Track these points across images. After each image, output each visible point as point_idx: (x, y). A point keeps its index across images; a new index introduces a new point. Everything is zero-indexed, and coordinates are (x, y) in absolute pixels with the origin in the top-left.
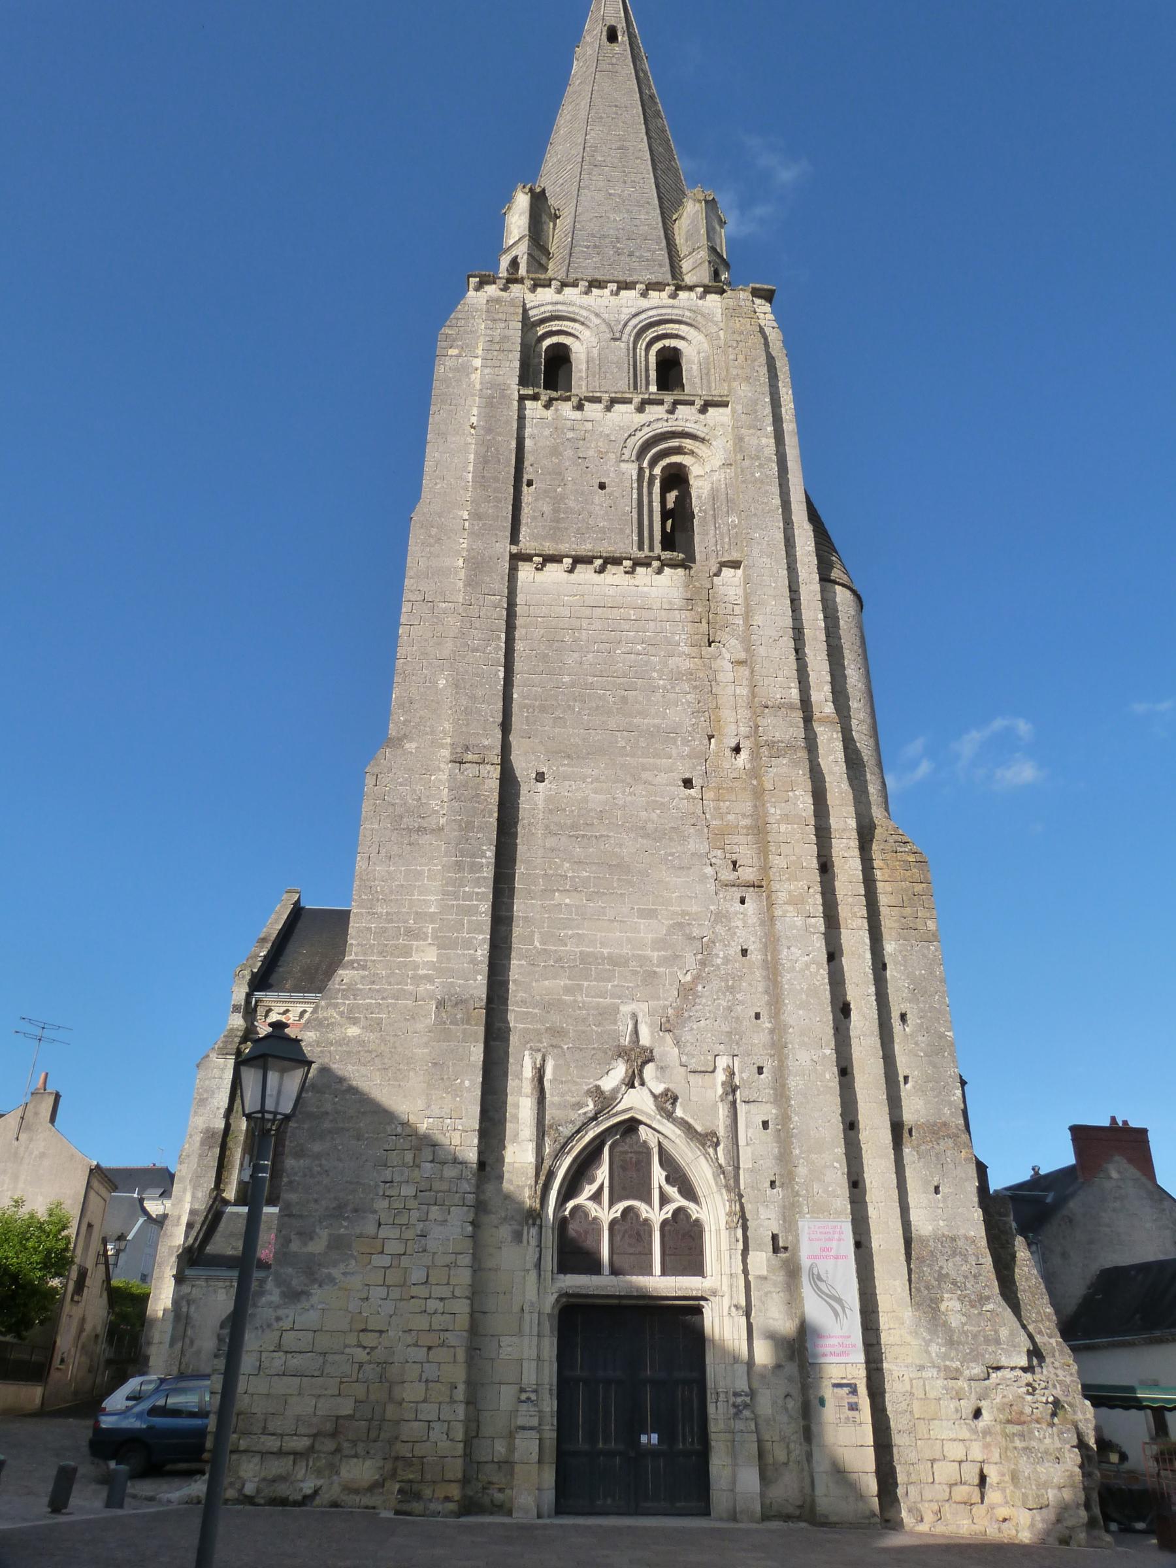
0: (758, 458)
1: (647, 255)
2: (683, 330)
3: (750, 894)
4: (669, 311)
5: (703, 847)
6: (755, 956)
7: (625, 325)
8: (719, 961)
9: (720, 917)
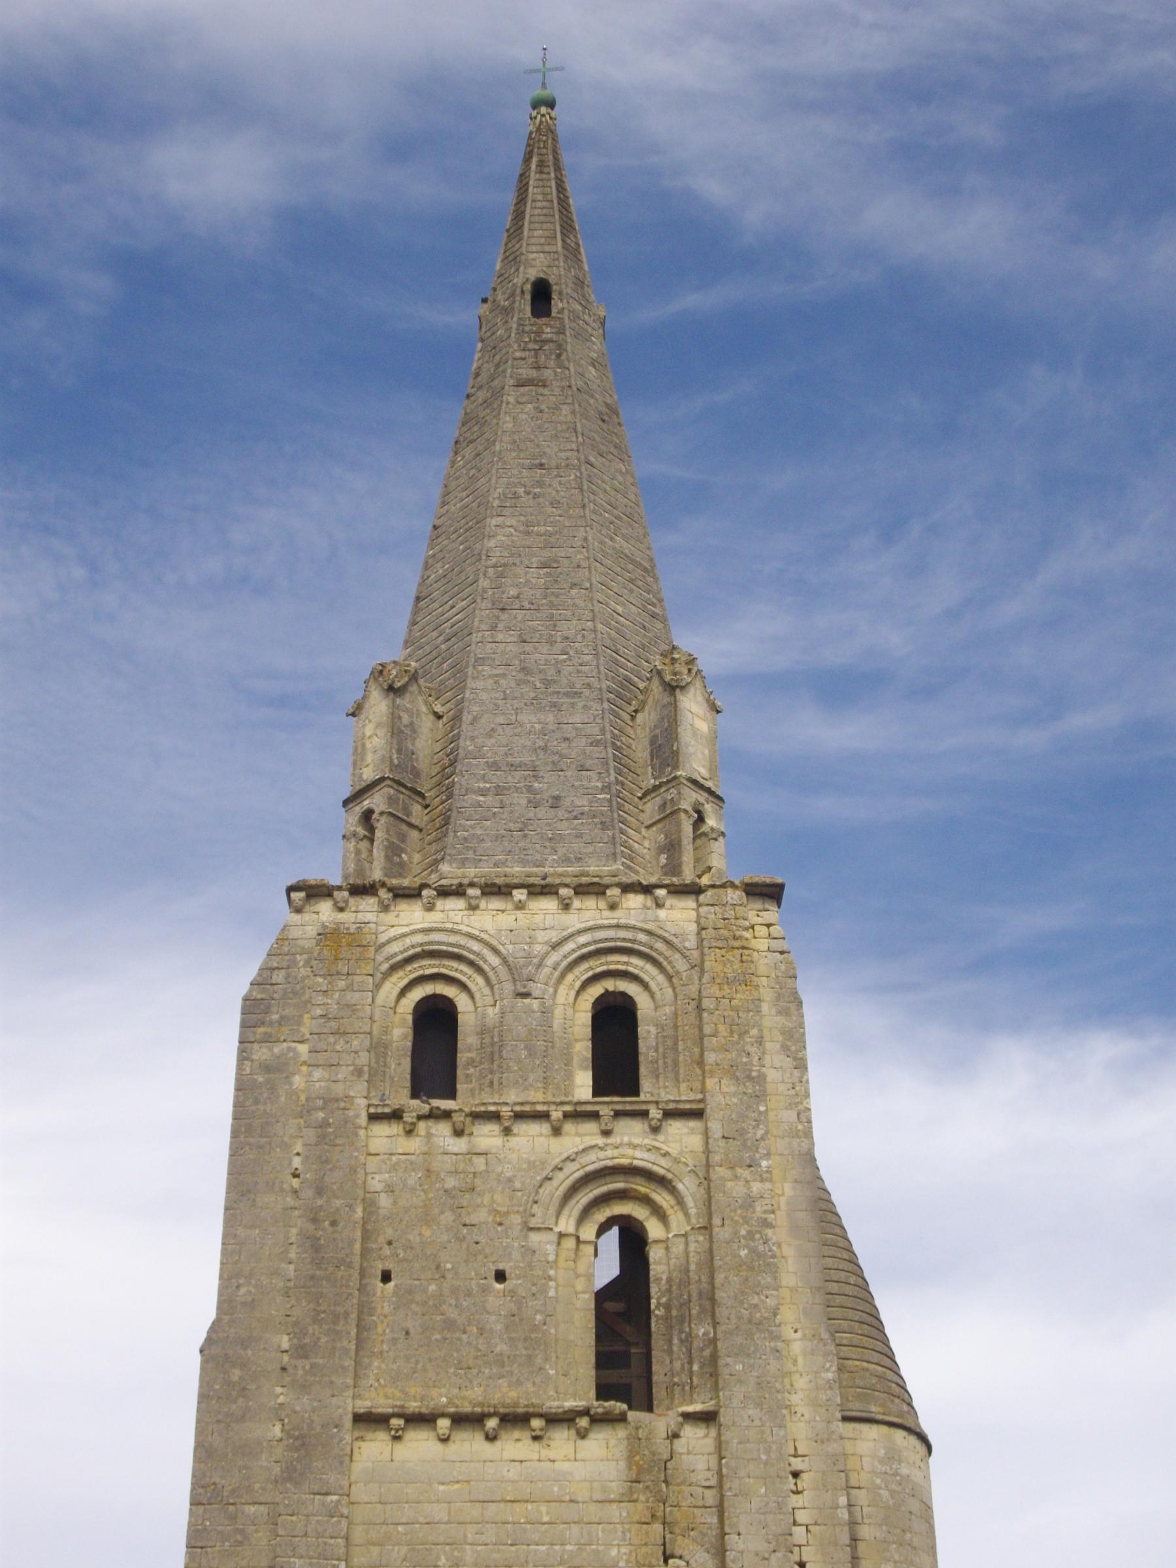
2: (636, 965)
4: (611, 933)
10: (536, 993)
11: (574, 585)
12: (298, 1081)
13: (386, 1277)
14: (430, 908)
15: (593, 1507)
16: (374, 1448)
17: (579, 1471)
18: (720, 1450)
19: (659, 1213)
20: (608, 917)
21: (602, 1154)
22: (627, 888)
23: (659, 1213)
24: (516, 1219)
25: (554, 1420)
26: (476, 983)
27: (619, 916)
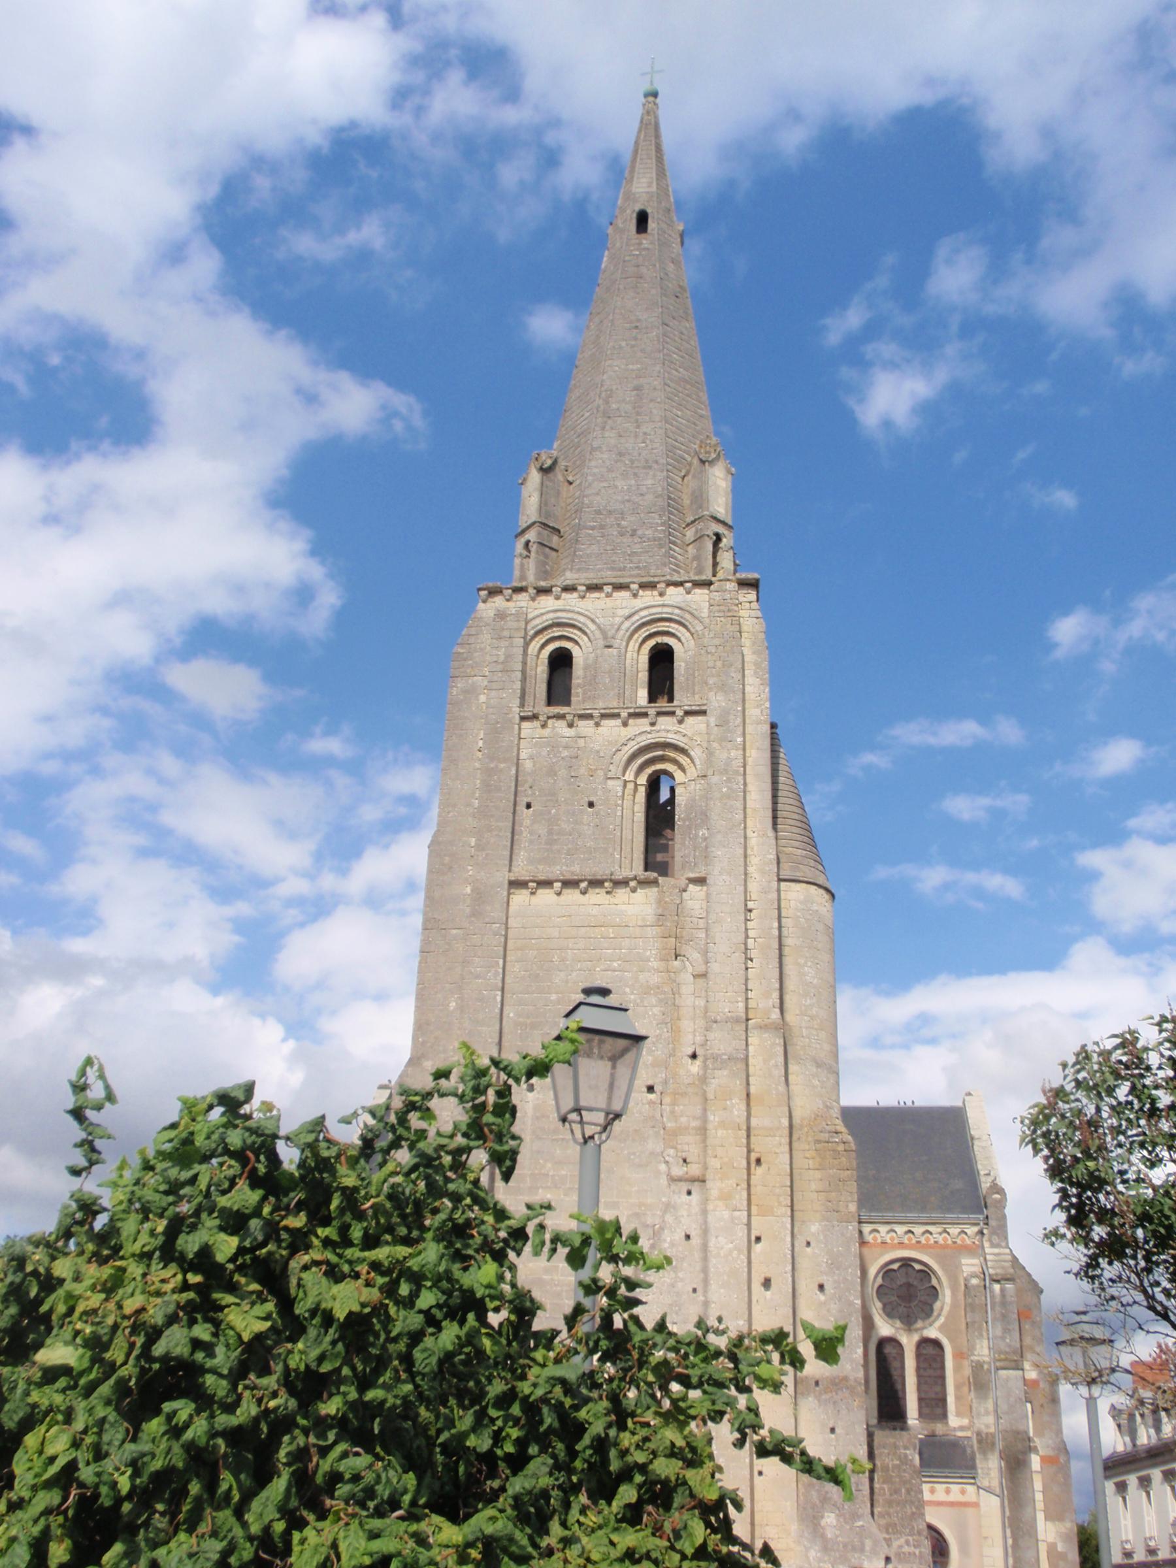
0: (726, 771)
1: (649, 532)
2: (673, 627)
3: (695, 1188)
4: (659, 610)
5: (659, 1148)
6: (696, 1241)
7: (618, 629)
8: (666, 1245)
9: (668, 1207)
10: (616, 645)
11: (651, 401)
12: (483, 698)
13: (529, 806)
14: (558, 598)
15: (638, 929)
16: (520, 898)
17: (631, 910)
18: (708, 898)
19: (682, 769)
20: (659, 600)
21: (649, 736)
22: (670, 584)
23: (682, 769)
24: (600, 773)
25: (624, 883)
26: (583, 640)
27: (666, 600)
